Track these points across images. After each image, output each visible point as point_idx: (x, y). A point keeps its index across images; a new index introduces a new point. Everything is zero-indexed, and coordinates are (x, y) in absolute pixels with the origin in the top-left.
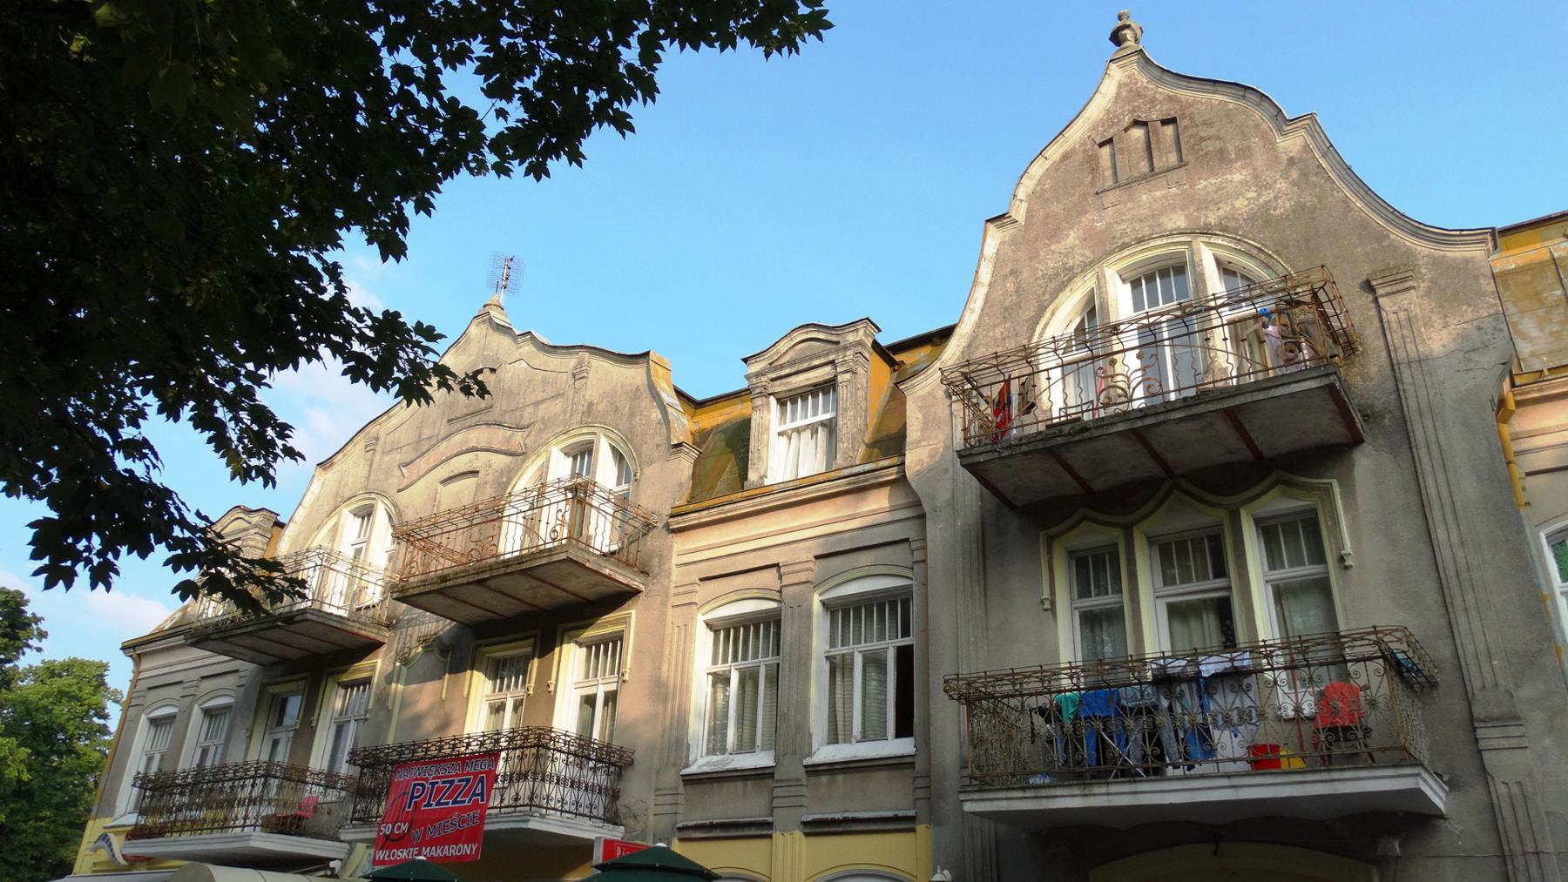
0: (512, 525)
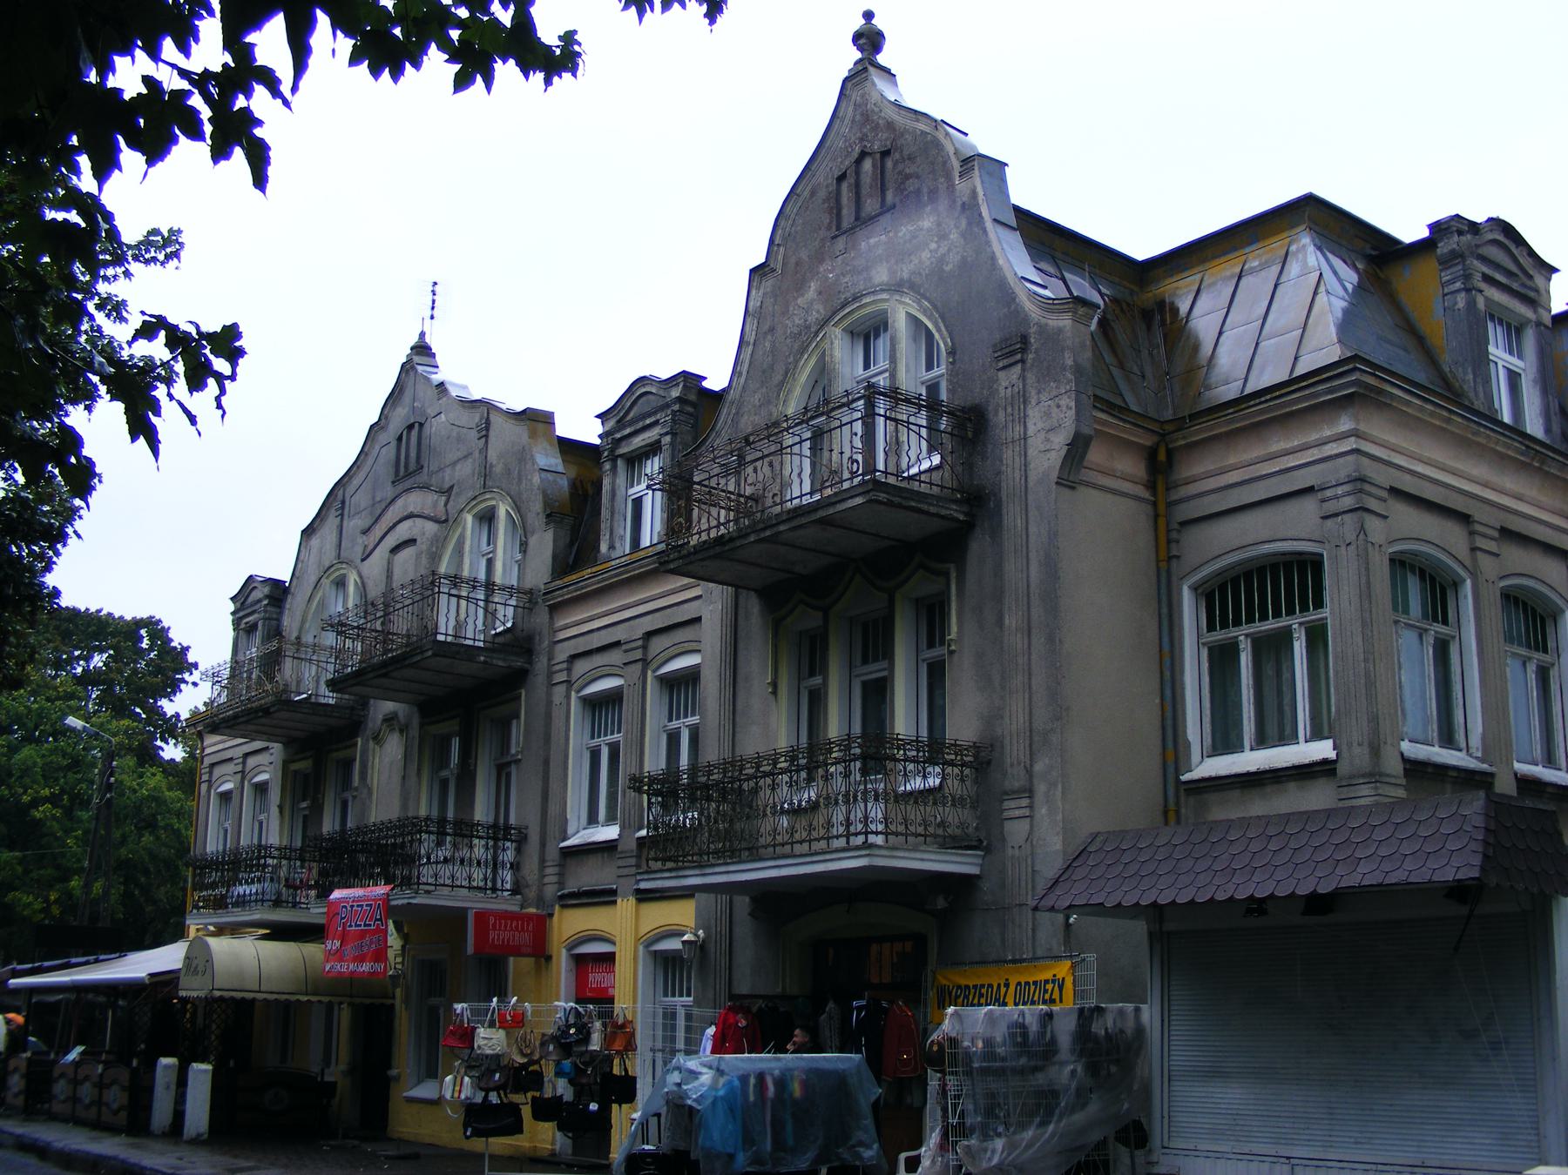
0: (796, 459)
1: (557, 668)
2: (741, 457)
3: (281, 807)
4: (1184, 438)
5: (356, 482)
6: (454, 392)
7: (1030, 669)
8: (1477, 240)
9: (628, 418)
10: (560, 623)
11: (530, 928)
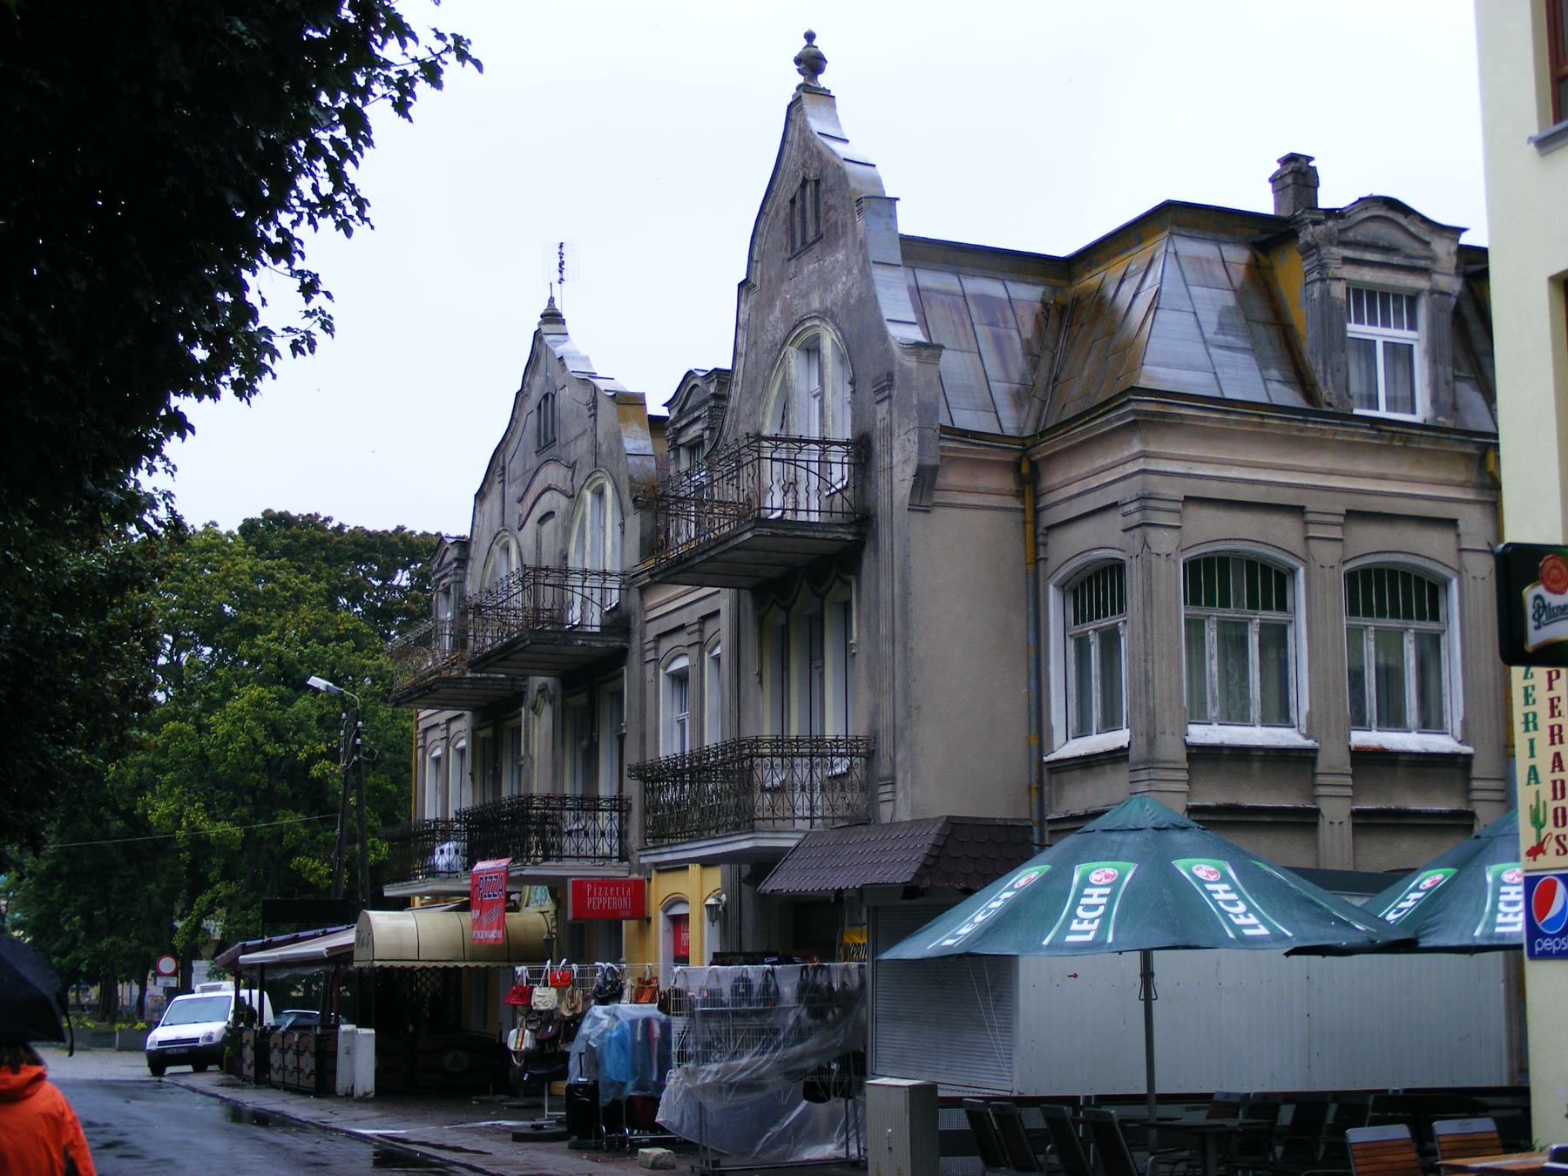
1: (648, 646)
2: (738, 461)
3: (472, 774)
4: (1039, 453)
5: (512, 448)
6: (572, 366)
7: (894, 673)
8: (1342, 224)
9: (687, 408)
10: (650, 603)
11: (628, 892)
